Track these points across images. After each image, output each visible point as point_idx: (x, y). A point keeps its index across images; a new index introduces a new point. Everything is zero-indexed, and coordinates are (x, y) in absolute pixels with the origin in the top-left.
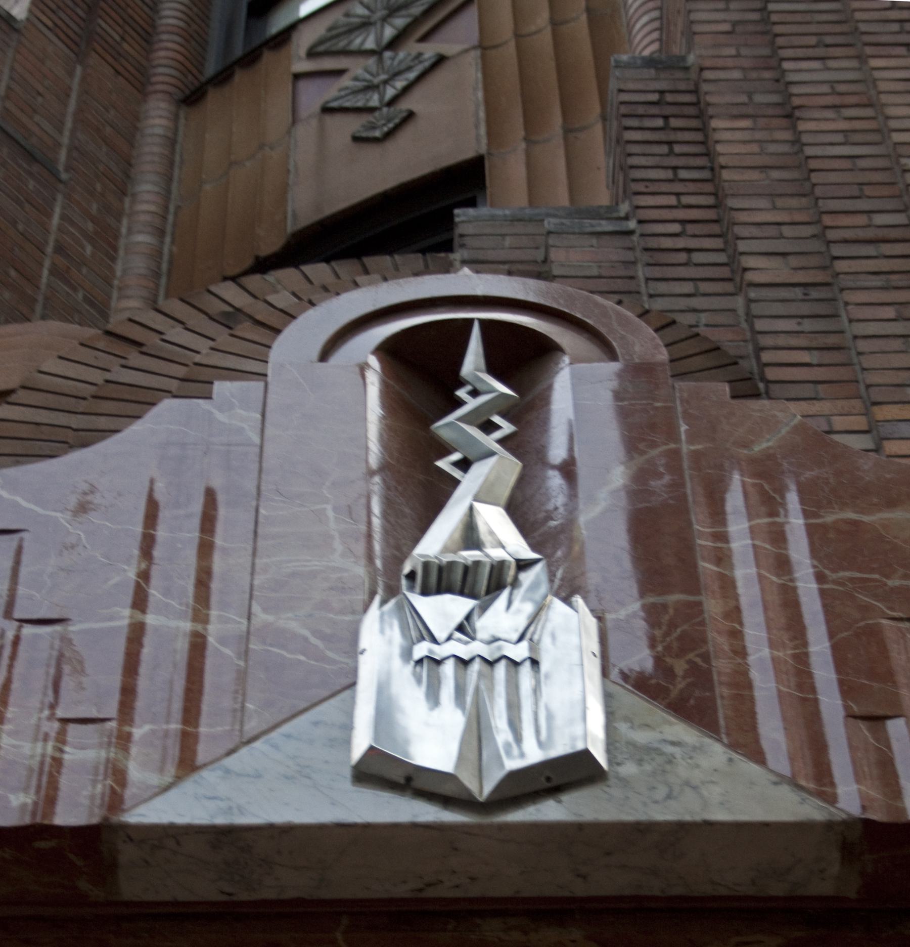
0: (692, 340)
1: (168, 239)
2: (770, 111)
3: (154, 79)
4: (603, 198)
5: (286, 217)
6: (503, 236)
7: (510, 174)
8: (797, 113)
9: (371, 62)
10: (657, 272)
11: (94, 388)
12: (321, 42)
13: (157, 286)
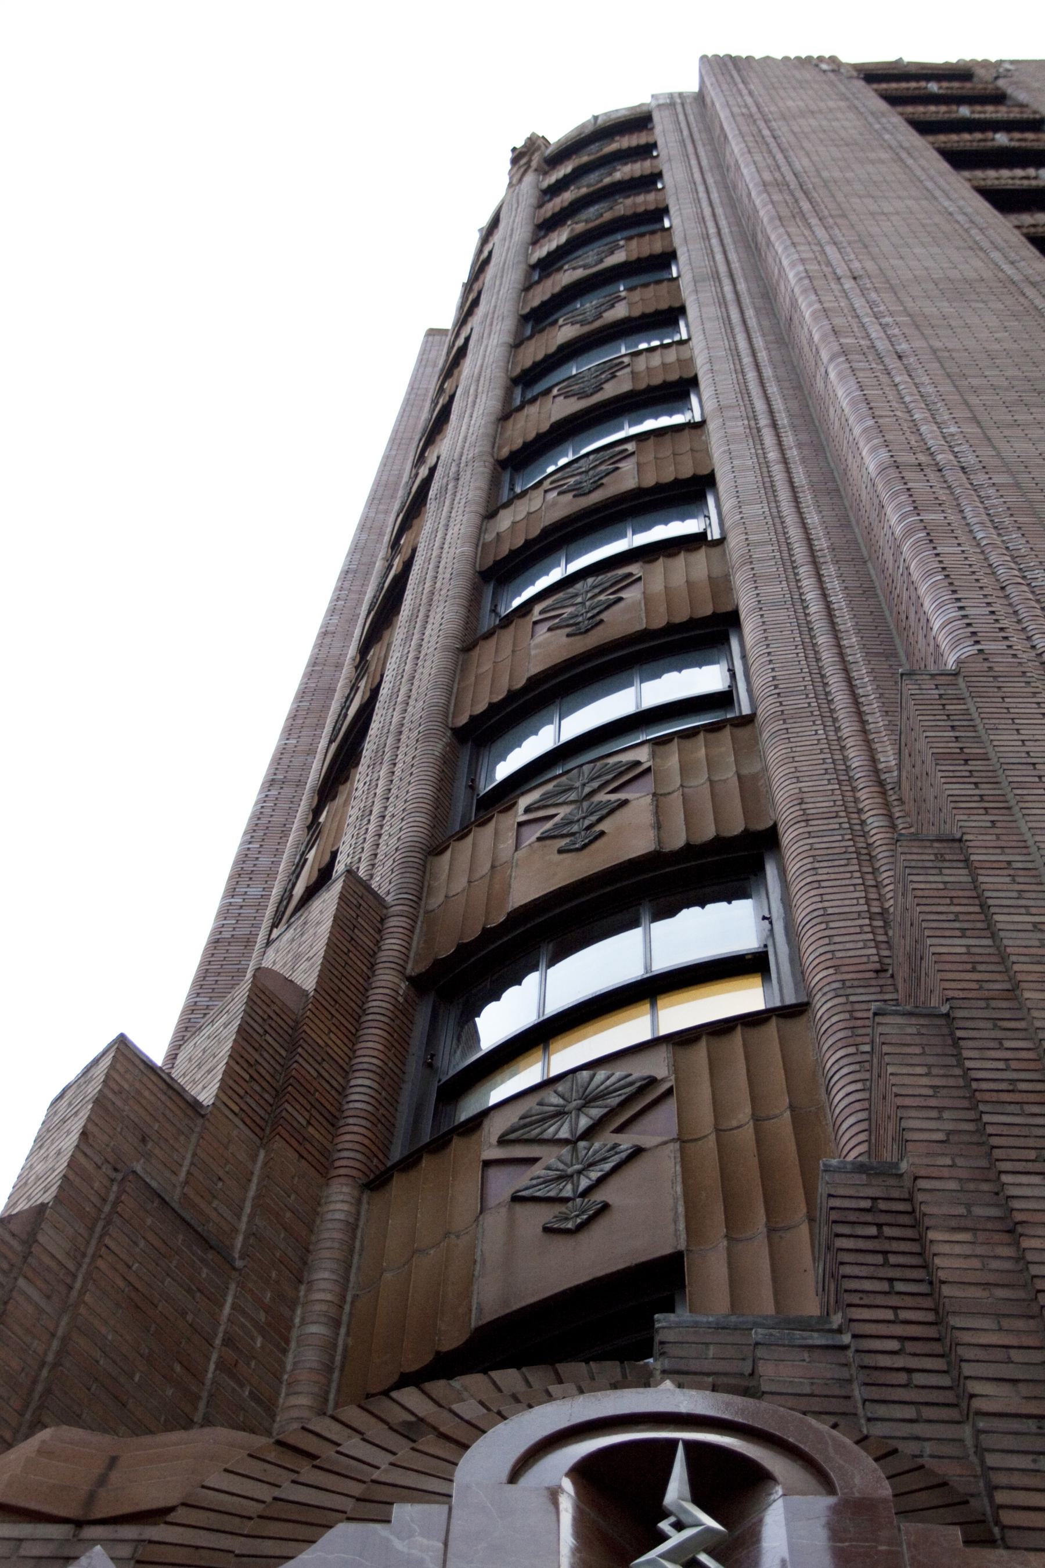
0: (916, 1473)
1: (343, 1331)
2: (989, 1226)
3: (338, 1164)
4: (812, 1308)
5: (471, 1310)
6: (707, 1344)
7: (711, 1271)
8: (1020, 1229)
9: (565, 1151)
10: (875, 1393)
11: (262, 1506)
12: (513, 1130)
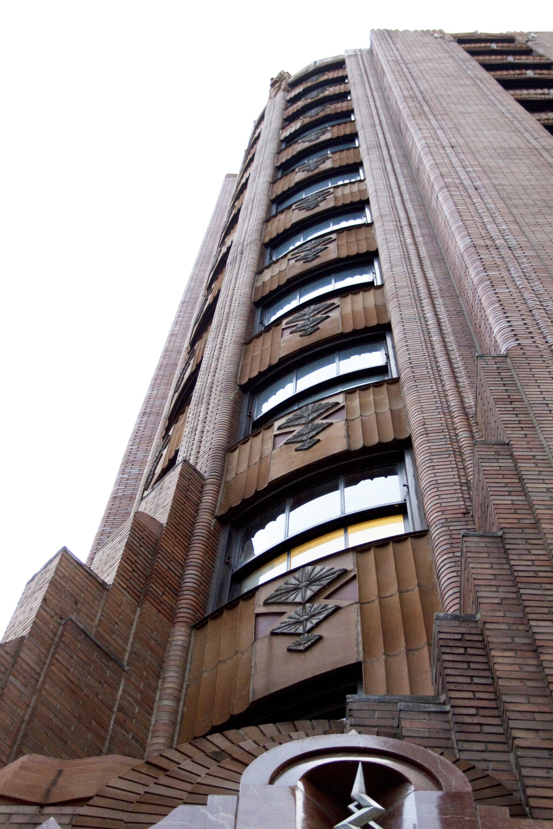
0: (485, 779)
1: (181, 703)
2: (524, 648)
3: (179, 615)
4: (430, 691)
5: (249, 693)
6: (374, 711)
7: (376, 672)
8: (540, 650)
9: (299, 608)
10: (463, 737)
11: (138, 796)
12: (272, 597)
13: (175, 730)
